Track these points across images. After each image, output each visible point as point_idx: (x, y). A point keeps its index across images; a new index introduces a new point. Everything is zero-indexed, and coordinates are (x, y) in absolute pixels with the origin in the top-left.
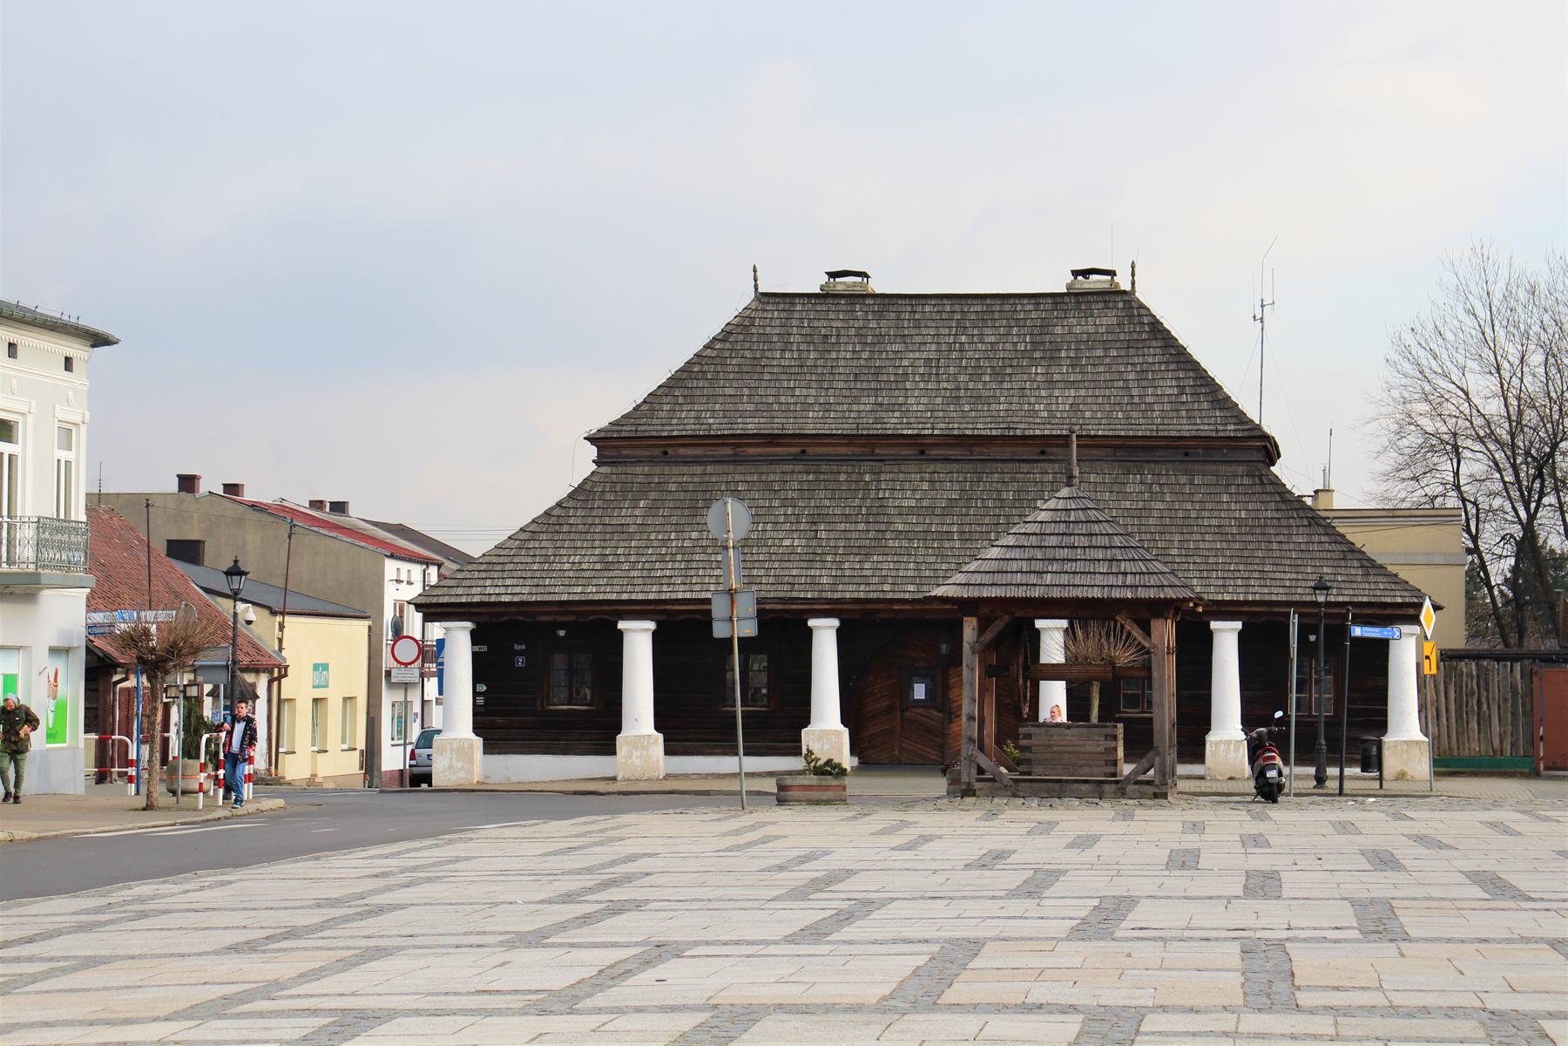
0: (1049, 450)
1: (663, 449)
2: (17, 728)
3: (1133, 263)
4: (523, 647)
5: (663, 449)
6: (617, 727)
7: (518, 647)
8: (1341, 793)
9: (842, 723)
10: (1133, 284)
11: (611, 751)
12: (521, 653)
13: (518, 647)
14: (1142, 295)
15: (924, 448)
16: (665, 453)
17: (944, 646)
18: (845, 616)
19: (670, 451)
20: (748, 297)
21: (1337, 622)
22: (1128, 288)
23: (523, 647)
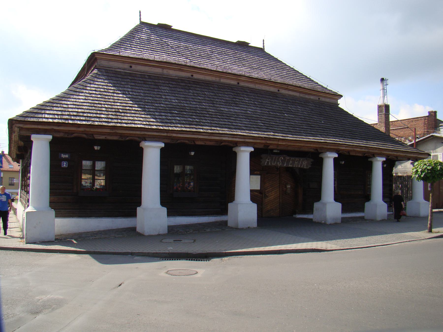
0: (280, 90)
1: (130, 65)
2: (190, 155)
3: (263, 40)
4: (67, 156)
5: (130, 65)
6: (139, 203)
7: (63, 156)
8: (9, 180)
9: (251, 200)
10: (264, 46)
11: (133, 214)
12: (65, 160)
13: (63, 156)
14: (267, 50)
15: (239, 82)
16: (131, 67)
17: (343, 162)
18: (256, 146)
19: (134, 67)
20: (138, 23)
21: (305, 164)
22: (262, 47)
23: (67, 156)
